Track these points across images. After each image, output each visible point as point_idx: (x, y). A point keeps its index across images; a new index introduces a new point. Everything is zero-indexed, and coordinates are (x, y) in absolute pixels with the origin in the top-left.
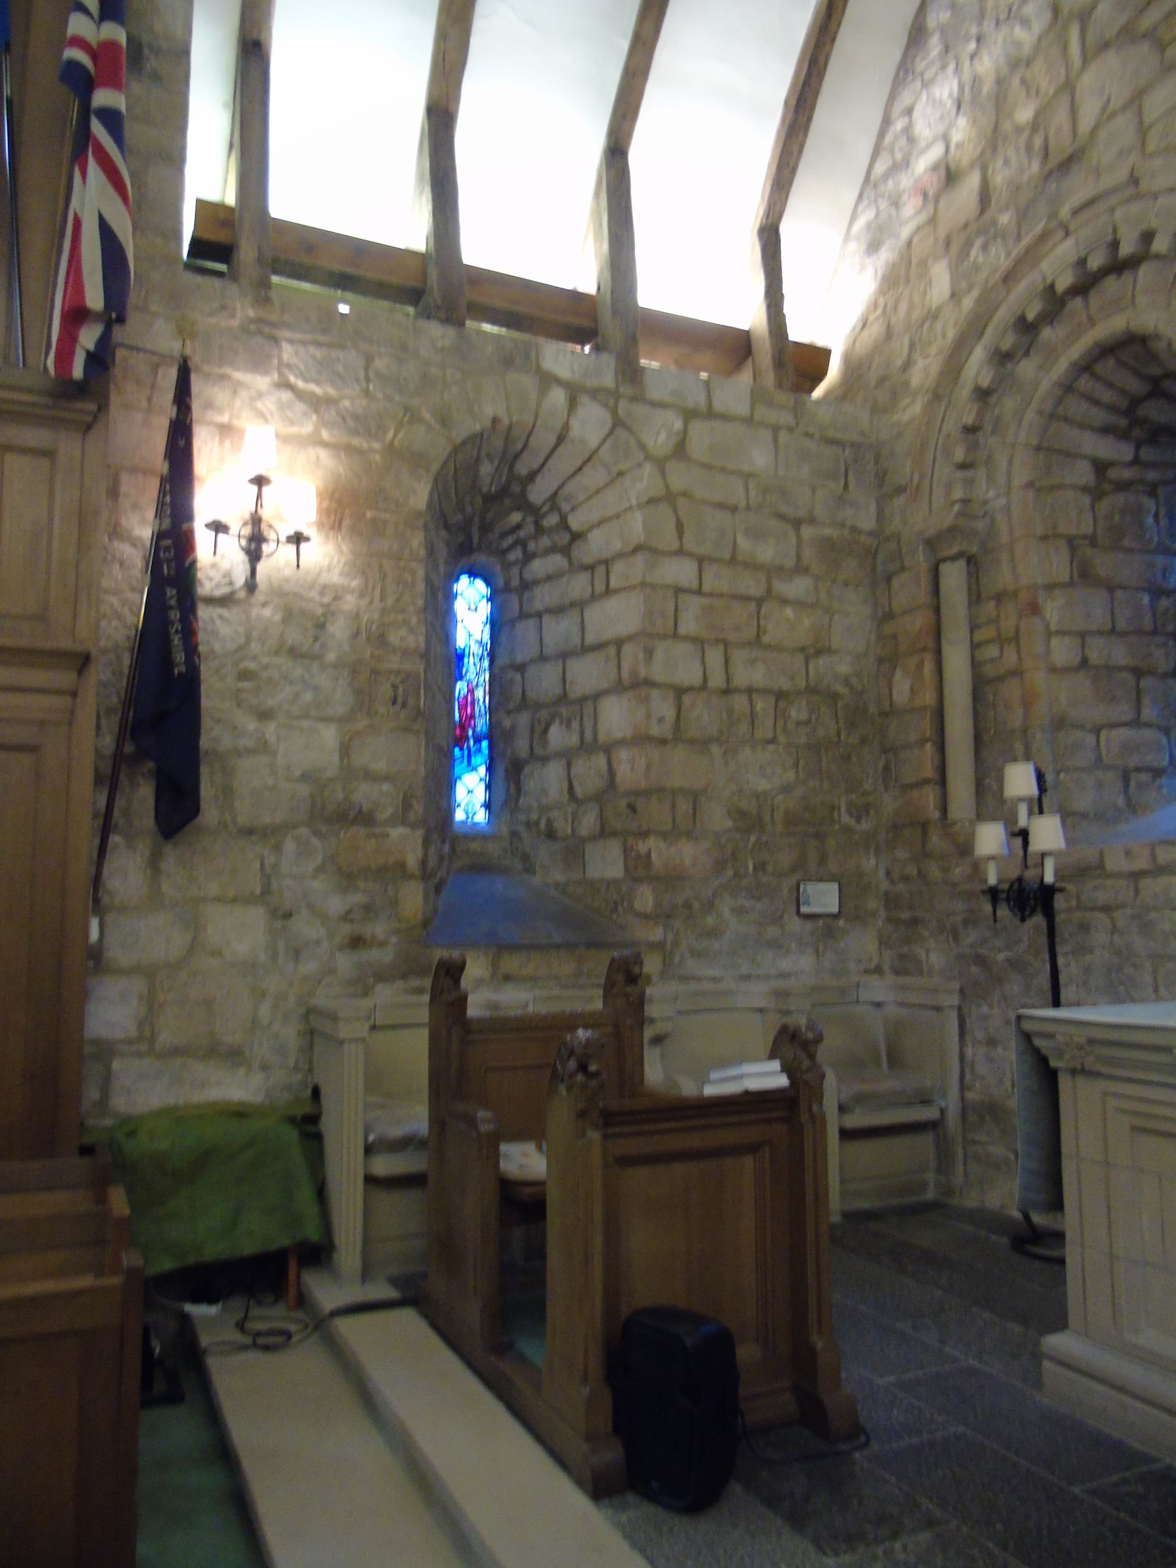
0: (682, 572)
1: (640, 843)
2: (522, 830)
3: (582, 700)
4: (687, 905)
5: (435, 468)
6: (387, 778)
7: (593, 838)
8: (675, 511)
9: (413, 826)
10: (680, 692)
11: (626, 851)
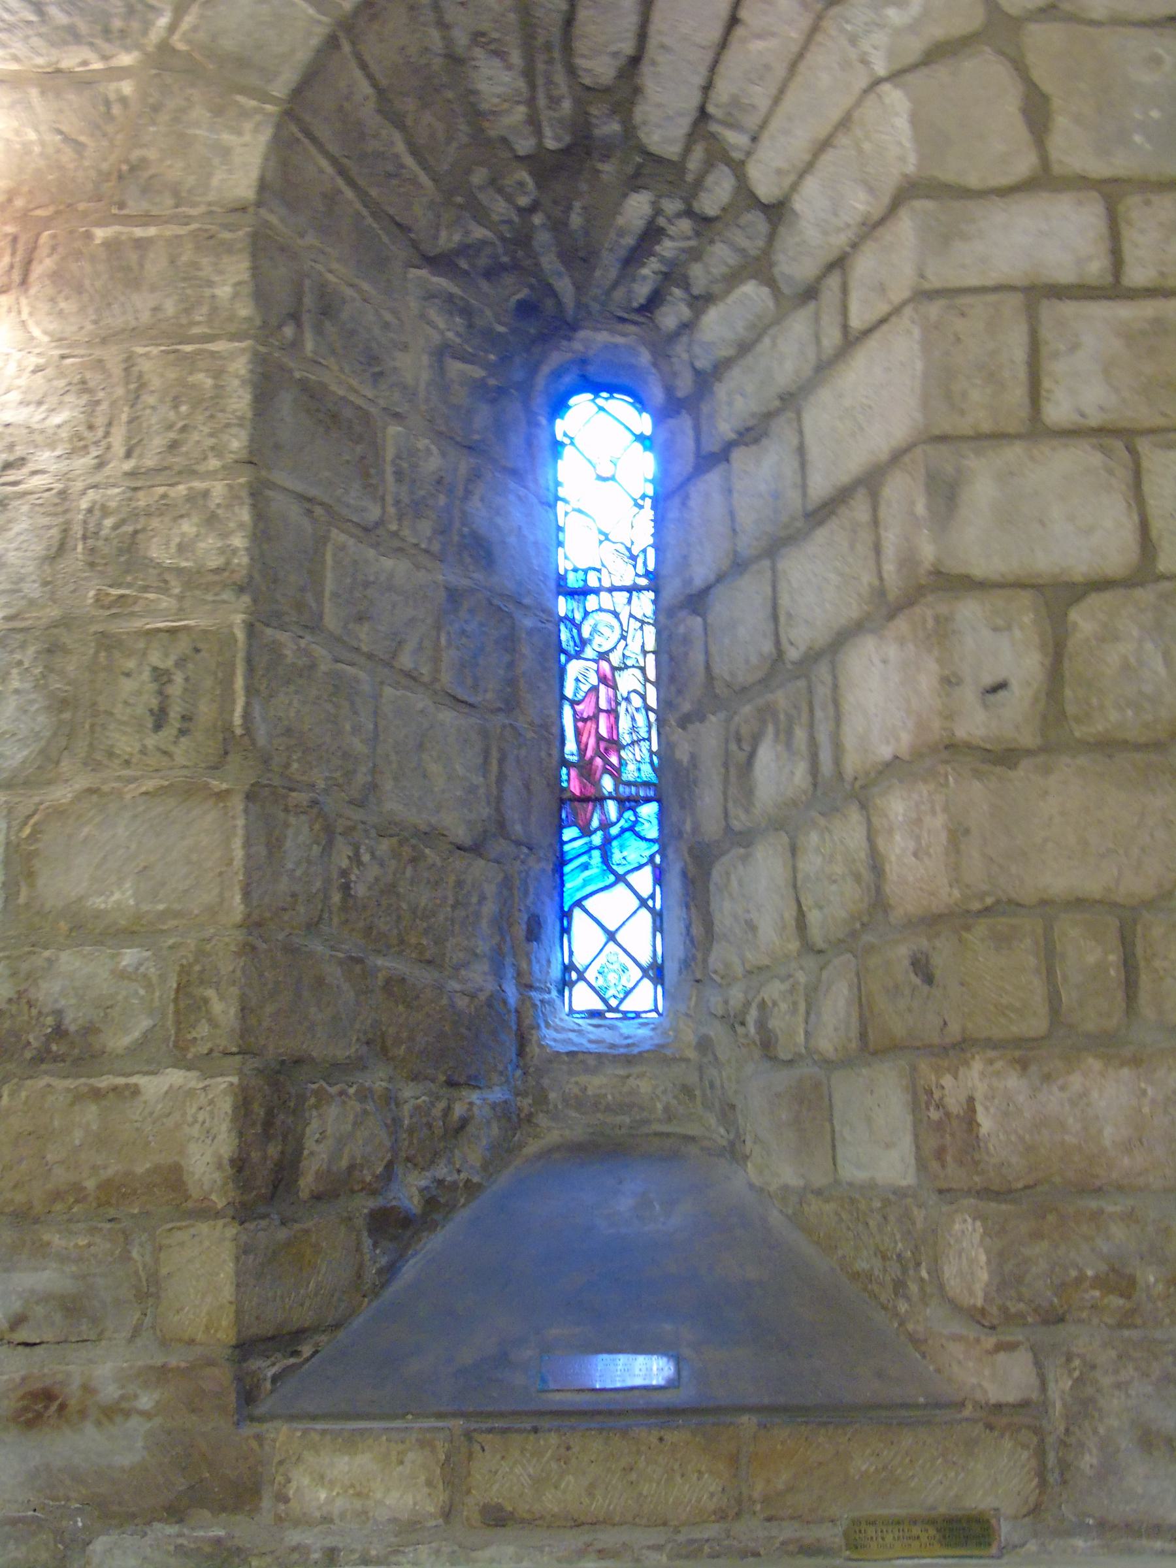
0: (1055, 237)
1: (947, 1081)
2: (716, 1031)
3: (813, 657)
4: (1118, 1280)
5: (280, 88)
6: (131, 931)
7: (846, 1062)
8: (1020, 68)
9: (205, 1064)
10: (1058, 597)
11: (921, 1099)
